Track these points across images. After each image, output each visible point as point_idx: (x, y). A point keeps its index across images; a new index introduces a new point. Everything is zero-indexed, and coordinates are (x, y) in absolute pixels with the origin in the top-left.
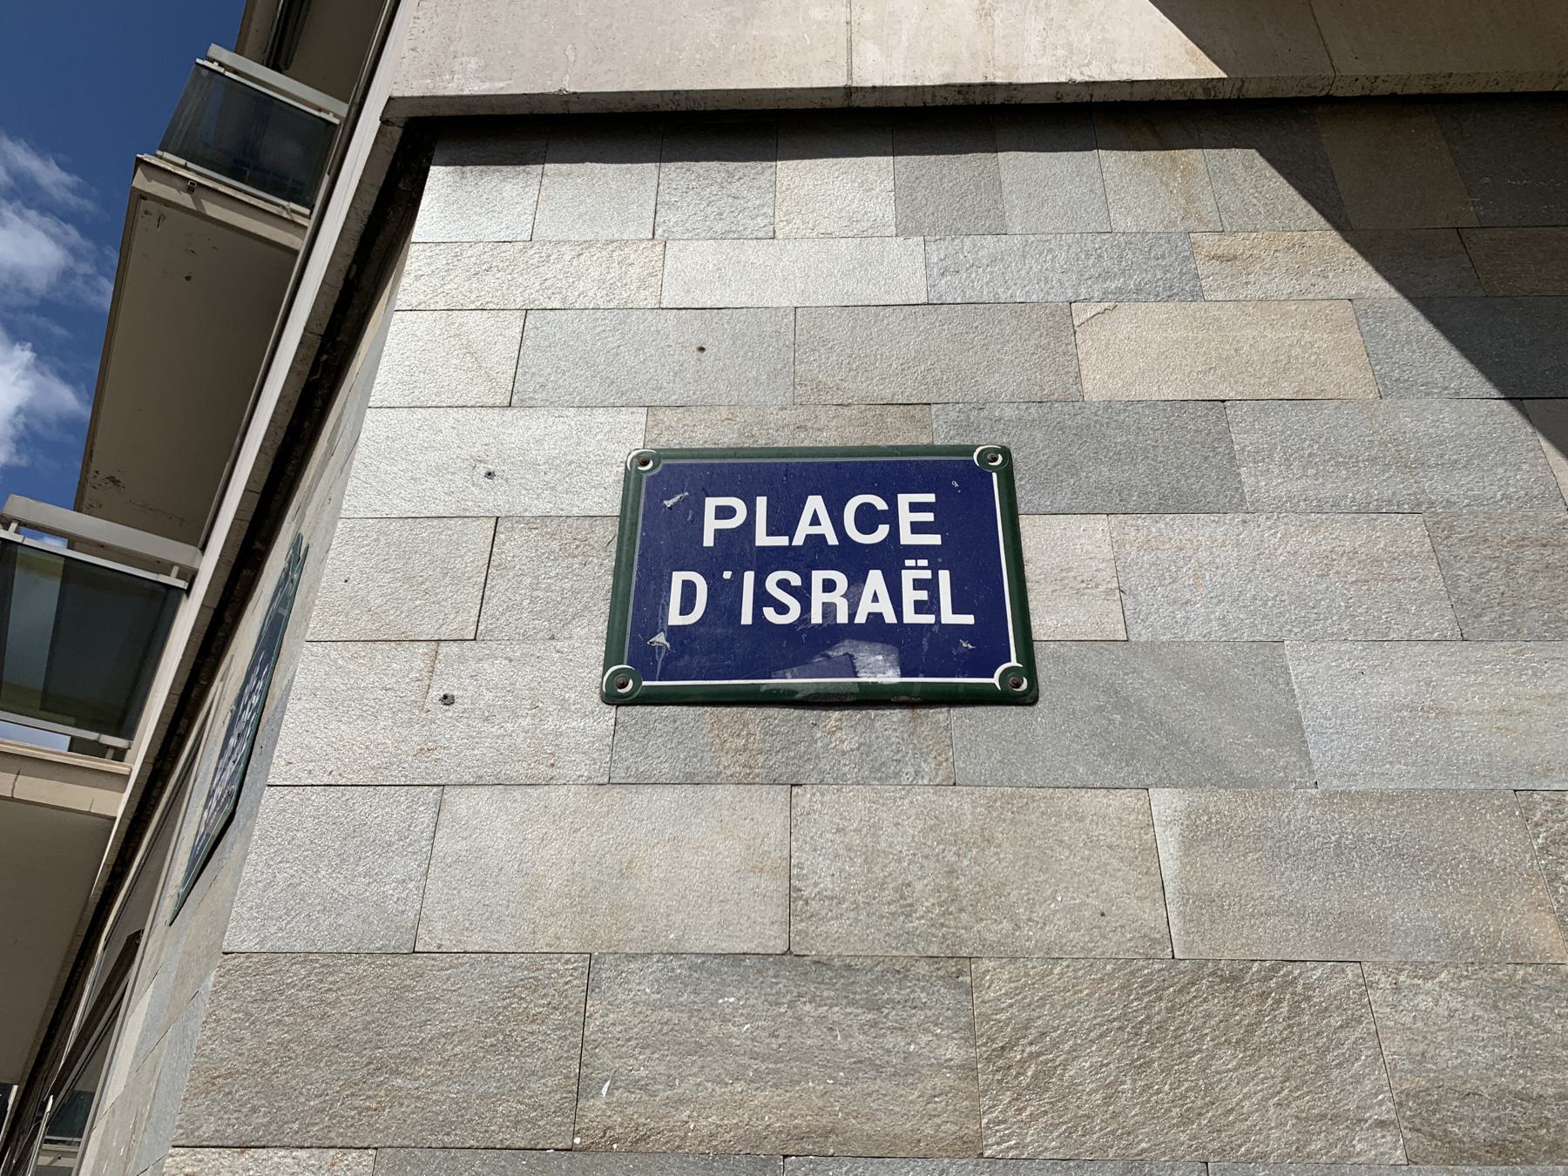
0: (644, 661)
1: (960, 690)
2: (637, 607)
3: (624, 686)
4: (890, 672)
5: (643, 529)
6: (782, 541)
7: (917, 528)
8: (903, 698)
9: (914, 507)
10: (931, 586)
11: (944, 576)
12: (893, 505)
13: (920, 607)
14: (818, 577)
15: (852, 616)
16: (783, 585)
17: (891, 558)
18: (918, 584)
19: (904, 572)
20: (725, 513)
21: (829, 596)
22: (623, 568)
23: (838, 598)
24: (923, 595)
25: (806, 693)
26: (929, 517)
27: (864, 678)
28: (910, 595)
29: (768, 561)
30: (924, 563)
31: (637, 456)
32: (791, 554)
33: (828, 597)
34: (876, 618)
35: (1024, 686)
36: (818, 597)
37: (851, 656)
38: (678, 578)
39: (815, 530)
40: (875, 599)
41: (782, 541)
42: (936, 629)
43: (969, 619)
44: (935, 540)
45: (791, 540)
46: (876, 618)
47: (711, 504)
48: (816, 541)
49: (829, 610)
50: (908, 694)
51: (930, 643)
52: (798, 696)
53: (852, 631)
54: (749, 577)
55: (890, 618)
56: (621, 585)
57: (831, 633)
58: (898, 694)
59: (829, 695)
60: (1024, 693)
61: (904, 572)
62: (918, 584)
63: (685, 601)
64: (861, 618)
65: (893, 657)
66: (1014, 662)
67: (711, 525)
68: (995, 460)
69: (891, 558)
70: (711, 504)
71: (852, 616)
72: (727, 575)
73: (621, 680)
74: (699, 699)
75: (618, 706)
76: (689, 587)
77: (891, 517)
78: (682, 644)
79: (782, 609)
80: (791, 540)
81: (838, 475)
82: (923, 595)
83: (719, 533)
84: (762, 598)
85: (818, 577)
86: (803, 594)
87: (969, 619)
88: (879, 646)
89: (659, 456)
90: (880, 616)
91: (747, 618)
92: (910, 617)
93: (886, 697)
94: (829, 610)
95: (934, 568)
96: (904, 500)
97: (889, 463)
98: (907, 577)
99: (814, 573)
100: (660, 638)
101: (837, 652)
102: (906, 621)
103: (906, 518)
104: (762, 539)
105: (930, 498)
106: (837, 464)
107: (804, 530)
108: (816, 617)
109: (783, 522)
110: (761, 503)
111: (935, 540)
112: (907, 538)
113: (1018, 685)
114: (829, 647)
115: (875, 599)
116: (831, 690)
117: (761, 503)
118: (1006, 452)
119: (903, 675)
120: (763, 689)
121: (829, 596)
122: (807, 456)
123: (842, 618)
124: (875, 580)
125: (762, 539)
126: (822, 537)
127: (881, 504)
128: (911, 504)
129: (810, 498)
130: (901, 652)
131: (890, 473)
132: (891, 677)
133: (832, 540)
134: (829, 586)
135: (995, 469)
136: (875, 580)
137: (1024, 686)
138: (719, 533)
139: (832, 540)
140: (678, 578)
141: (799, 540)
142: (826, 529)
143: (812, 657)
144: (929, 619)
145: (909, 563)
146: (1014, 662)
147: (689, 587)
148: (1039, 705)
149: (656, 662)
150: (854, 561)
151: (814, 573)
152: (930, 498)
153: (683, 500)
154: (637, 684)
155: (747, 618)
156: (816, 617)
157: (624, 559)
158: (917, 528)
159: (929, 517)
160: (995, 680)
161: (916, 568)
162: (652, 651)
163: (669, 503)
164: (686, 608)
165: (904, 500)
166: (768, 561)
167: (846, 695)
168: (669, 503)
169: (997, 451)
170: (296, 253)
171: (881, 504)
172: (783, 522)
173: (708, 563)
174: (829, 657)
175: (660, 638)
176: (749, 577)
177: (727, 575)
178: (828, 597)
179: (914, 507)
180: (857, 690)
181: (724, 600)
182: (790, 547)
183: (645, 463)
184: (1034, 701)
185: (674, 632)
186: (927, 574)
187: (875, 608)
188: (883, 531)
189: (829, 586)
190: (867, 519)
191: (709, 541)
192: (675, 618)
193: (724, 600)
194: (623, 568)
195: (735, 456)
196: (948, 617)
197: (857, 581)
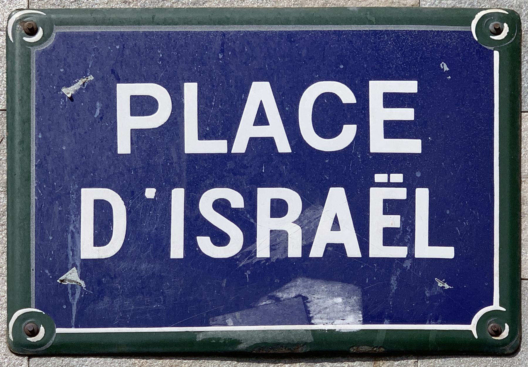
0: (55, 303)
1: (431, 337)
2: (41, 236)
3: (34, 333)
4: (351, 318)
5: (39, 129)
6: (218, 147)
7: (393, 130)
8: (365, 349)
9: (391, 100)
10: (404, 208)
11: (422, 196)
12: (363, 96)
13: (390, 237)
14: (265, 196)
15: (307, 248)
16: (221, 206)
17: (356, 171)
18: (390, 207)
19: (372, 190)
20: (143, 106)
21: (280, 222)
22: (18, 183)
23: (288, 224)
24: (394, 221)
25: (250, 343)
26: (407, 114)
27: (320, 325)
28: (379, 221)
29: (202, 173)
30: (397, 178)
31: (21, 21)
32: (230, 165)
33: (278, 224)
34: (336, 250)
35: (505, 334)
36: (265, 224)
37: (305, 298)
38: (89, 196)
39: (262, 132)
40: (336, 225)
41: (218, 147)
42: (408, 264)
43: (447, 252)
44: (413, 146)
45: (230, 146)
46: (336, 250)
47: (125, 92)
48: (262, 146)
49: (278, 239)
50: (369, 343)
51: (399, 281)
52: (241, 347)
53: (307, 267)
54: (178, 196)
55: (353, 251)
56: (18, 206)
57: (282, 269)
58: (358, 343)
59: (277, 345)
60: (504, 342)
61: (372, 190)
62: (390, 207)
63: (99, 227)
64: (317, 251)
65: (355, 299)
66: (496, 306)
67: (126, 123)
68: (499, 31)
69: (356, 171)
70: (125, 92)
71: (307, 248)
72: (150, 193)
73: (30, 327)
74: (126, 349)
75: (30, 356)
76: (103, 209)
77: (359, 114)
78: (99, 282)
79: (221, 238)
80: (230, 146)
81: (292, 56)
82: (394, 221)
83: (137, 135)
84: (196, 225)
85: (265, 196)
86: (246, 219)
87: (447, 252)
88: (338, 287)
89: (51, 20)
90: (340, 248)
91: (177, 251)
92: (378, 249)
93: (345, 348)
94: (278, 239)
95: (410, 185)
96: (377, 89)
97: (359, 34)
98: (377, 197)
99: (372, 84)
100: (73, 276)
101: (288, 294)
102: (418, 254)
103: (379, 114)
104: (193, 144)
105: (410, 87)
106: (290, 36)
107: (246, 131)
108: (263, 250)
109: (220, 120)
110: (191, 90)
111: (413, 146)
112: (379, 144)
113: (498, 333)
114: (279, 287)
115: (336, 225)
116: (280, 339)
117: (191, 90)
118: (514, 20)
119: (365, 321)
120: (200, 337)
121: (280, 222)
122: (249, 23)
123: (295, 251)
124: (337, 199)
125: (193, 144)
126: (271, 141)
127: (347, 96)
128: (385, 95)
129: (255, 85)
130: (364, 293)
131: (359, 51)
132: (351, 323)
133: (283, 146)
134: (279, 208)
135: (497, 44)
136: (337, 199)
137: (505, 334)
138: (137, 135)
139: (283, 146)
140: (89, 196)
141: (240, 146)
142: (276, 130)
143: (257, 298)
144: (400, 252)
145: (380, 178)
146: (496, 306)
147: (103, 209)
148: (520, 356)
149: (69, 305)
150: (310, 174)
151: (372, 84)
152: (410, 87)
153: (88, 87)
154: (50, 332)
155: (177, 251)
156: (263, 250)
157: (18, 171)
158: (393, 130)
159: (407, 114)
160: (472, 327)
161: (389, 184)
162: (64, 291)
163: (69, 91)
164: (102, 236)
165: (377, 89)
166: (202, 173)
167: (298, 345)
168: (69, 91)
169: (502, 18)
170: (309, 321)
171: (347, 96)
172: (220, 120)
173: (127, 177)
174: (278, 300)
175: (73, 276)
176: (178, 196)
177: (150, 193)
178: (278, 224)
179: (391, 100)
180: (310, 339)
181: (147, 225)
182: (229, 156)
183: (32, 32)
184: (511, 348)
185: (89, 267)
186: (401, 194)
187: (336, 238)
188: (349, 133)
189: (279, 208)
190: (330, 113)
191: (124, 147)
192: (88, 250)
193: (147, 225)
194: (18, 183)
195: (153, 22)
196: (424, 249)
197: (314, 200)
